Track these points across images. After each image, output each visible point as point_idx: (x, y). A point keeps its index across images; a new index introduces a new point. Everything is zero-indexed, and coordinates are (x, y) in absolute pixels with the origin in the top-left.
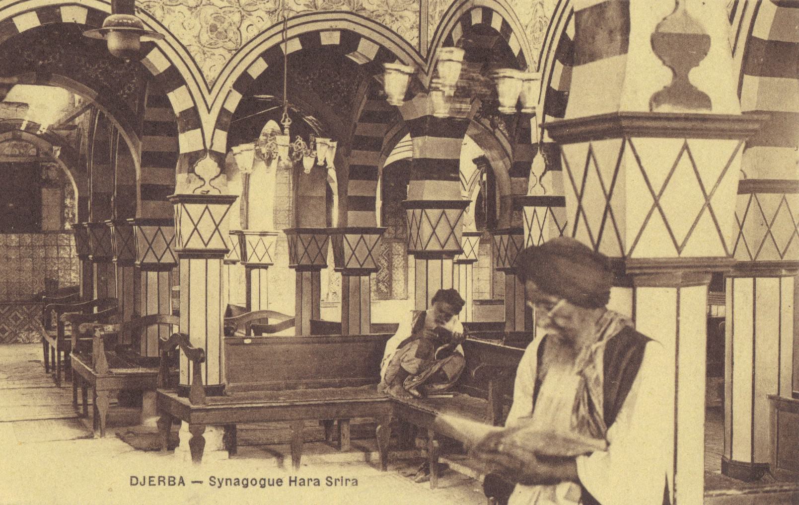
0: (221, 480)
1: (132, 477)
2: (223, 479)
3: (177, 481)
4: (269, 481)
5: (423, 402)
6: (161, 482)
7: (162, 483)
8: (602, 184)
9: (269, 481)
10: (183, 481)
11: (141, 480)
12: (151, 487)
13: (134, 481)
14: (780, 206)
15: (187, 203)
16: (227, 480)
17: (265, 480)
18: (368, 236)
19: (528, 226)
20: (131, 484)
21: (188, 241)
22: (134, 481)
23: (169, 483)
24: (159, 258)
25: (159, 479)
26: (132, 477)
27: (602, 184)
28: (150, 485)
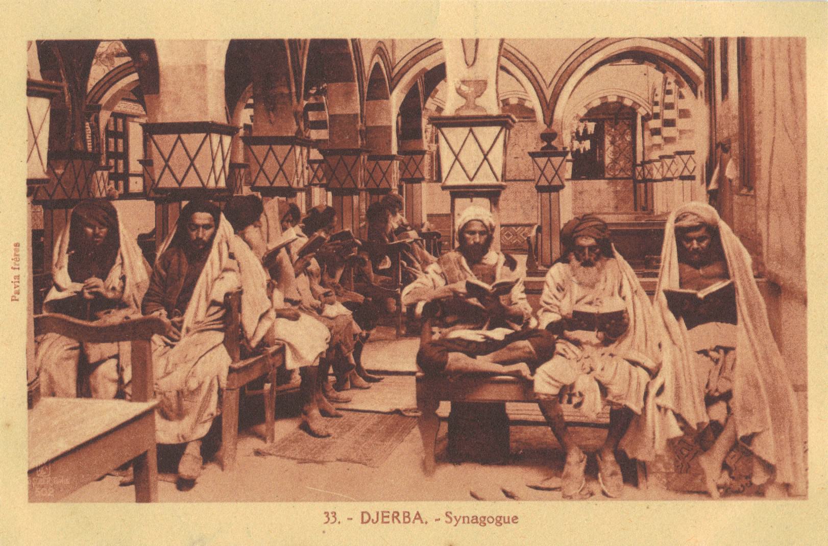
0: (458, 518)
1: (363, 513)
2: (460, 517)
3: (412, 516)
4: (504, 519)
5: (293, 434)
6: (395, 520)
7: (395, 520)
8: (446, 140)
9: (504, 519)
10: (420, 517)
11: (374, 517)
12: (384, 524)
13: (366, 517)
14: (338, 164)
15: (443, 127)
16: (464, 517)
17: (405, 522)
18: (373, 187)
19: (222, 148)
20: (363, 522)
21: (203, 143)
22: (366, 517)
23: (383, 519)
24: (271, 180)
25: (404, 514)
26: (363, 513)
27: (446, 140)
28: (383, 522)
